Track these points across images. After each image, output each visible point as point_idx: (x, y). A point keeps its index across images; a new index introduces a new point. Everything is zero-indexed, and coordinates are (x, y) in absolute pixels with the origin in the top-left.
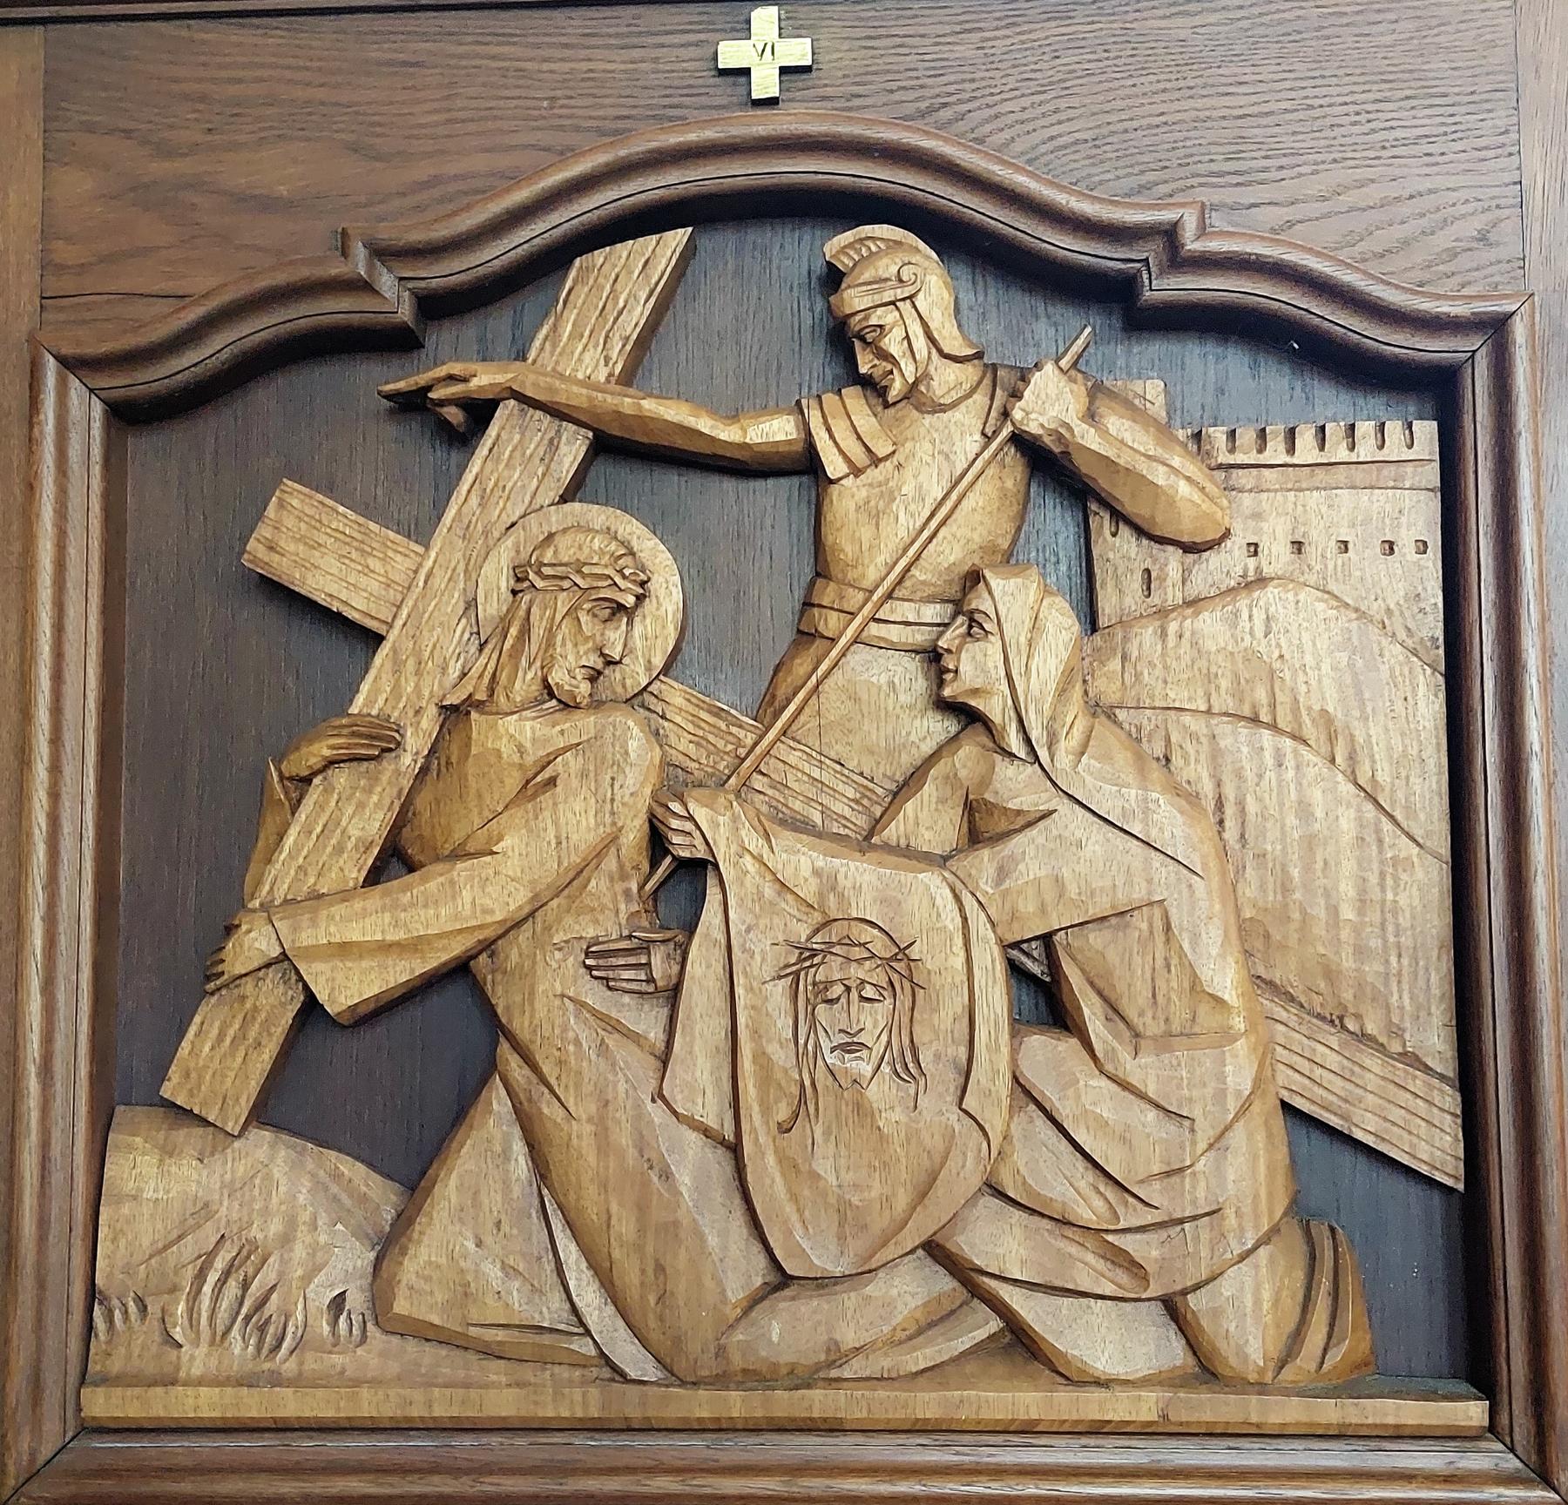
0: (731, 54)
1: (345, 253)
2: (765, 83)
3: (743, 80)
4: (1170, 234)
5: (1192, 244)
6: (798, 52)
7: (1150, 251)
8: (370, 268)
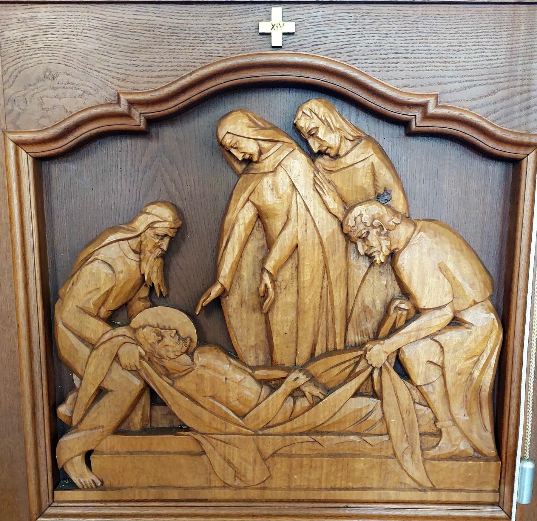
0: (264, 27)
1: (119, 102)
2: (277, 40)
3: (269, 36)
4: (424, 106)
5: (431, 110)
6: (290, 27)
7: (418, 113)
8: (129, 109)
